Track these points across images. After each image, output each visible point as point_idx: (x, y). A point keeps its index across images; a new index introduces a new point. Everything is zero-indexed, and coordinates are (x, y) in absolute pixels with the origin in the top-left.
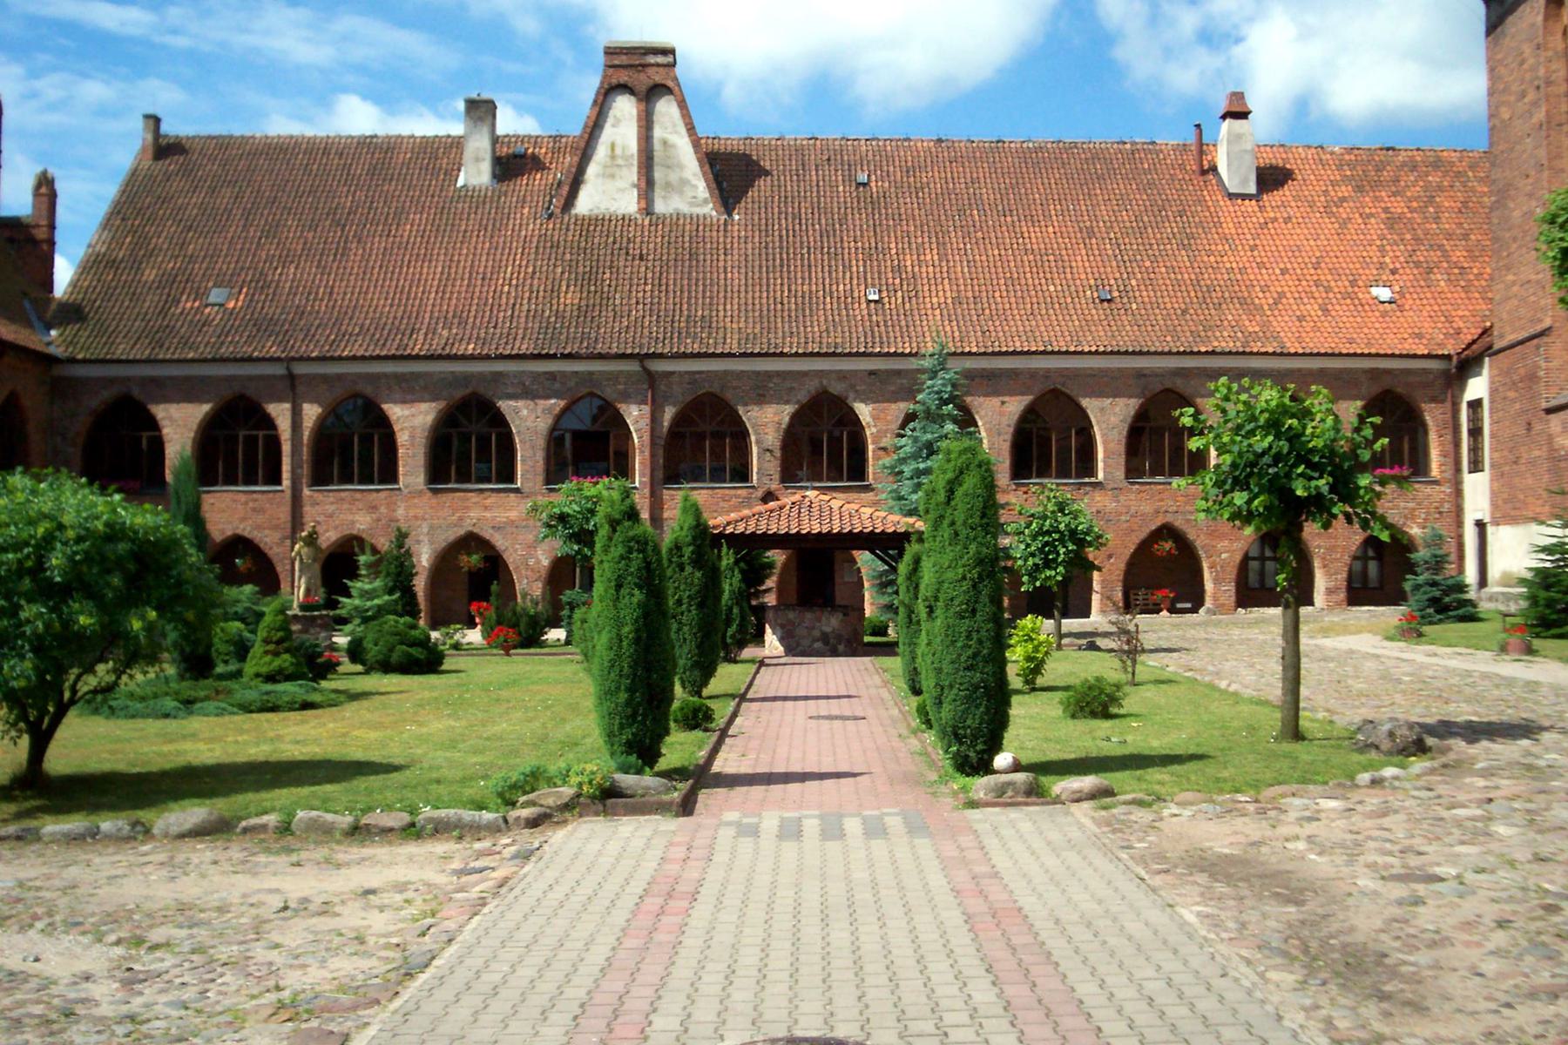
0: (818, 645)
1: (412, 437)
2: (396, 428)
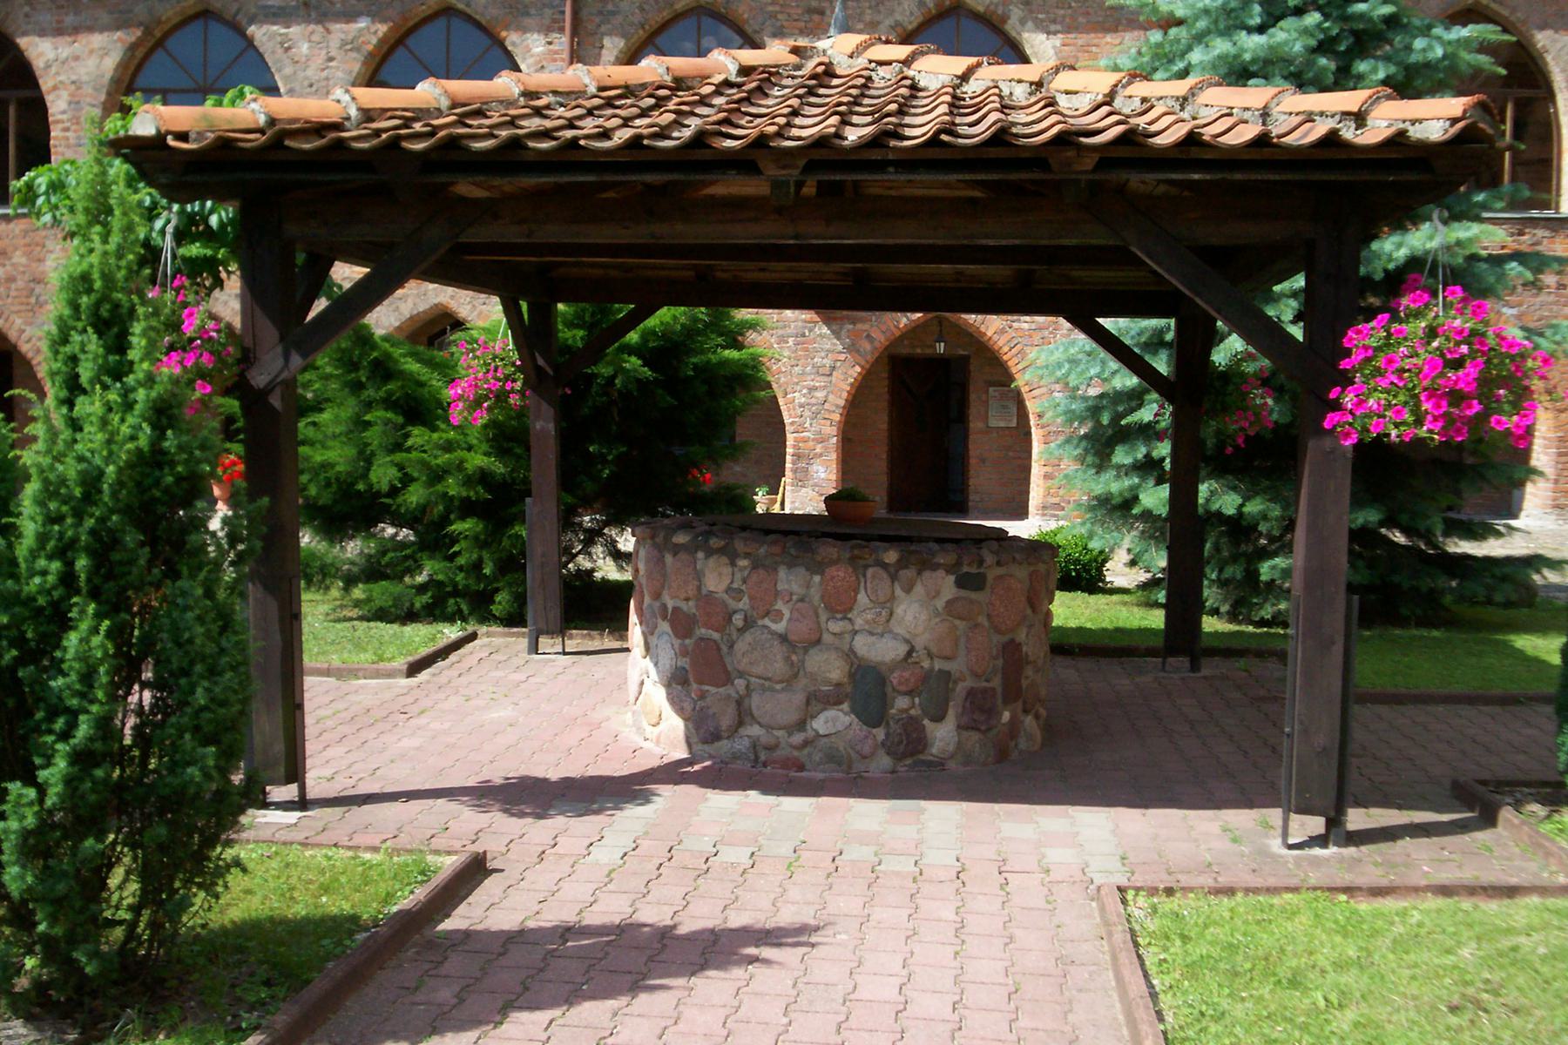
0: (833, 722)
1: (75, 103)
2: (45, 84)
